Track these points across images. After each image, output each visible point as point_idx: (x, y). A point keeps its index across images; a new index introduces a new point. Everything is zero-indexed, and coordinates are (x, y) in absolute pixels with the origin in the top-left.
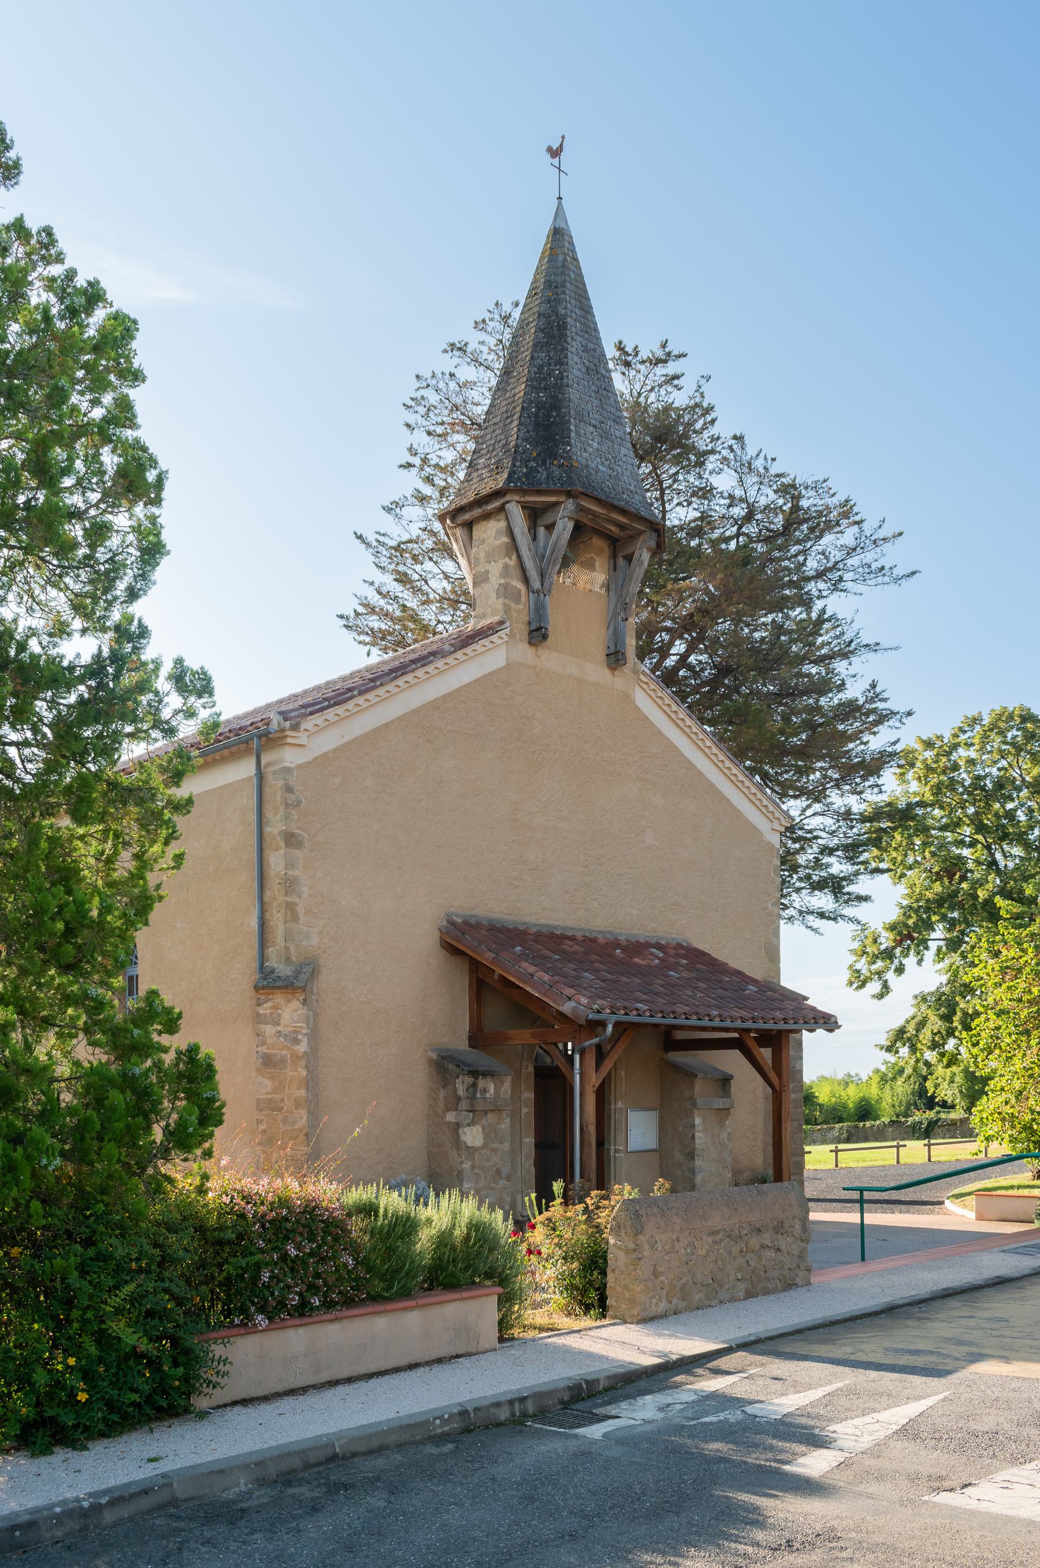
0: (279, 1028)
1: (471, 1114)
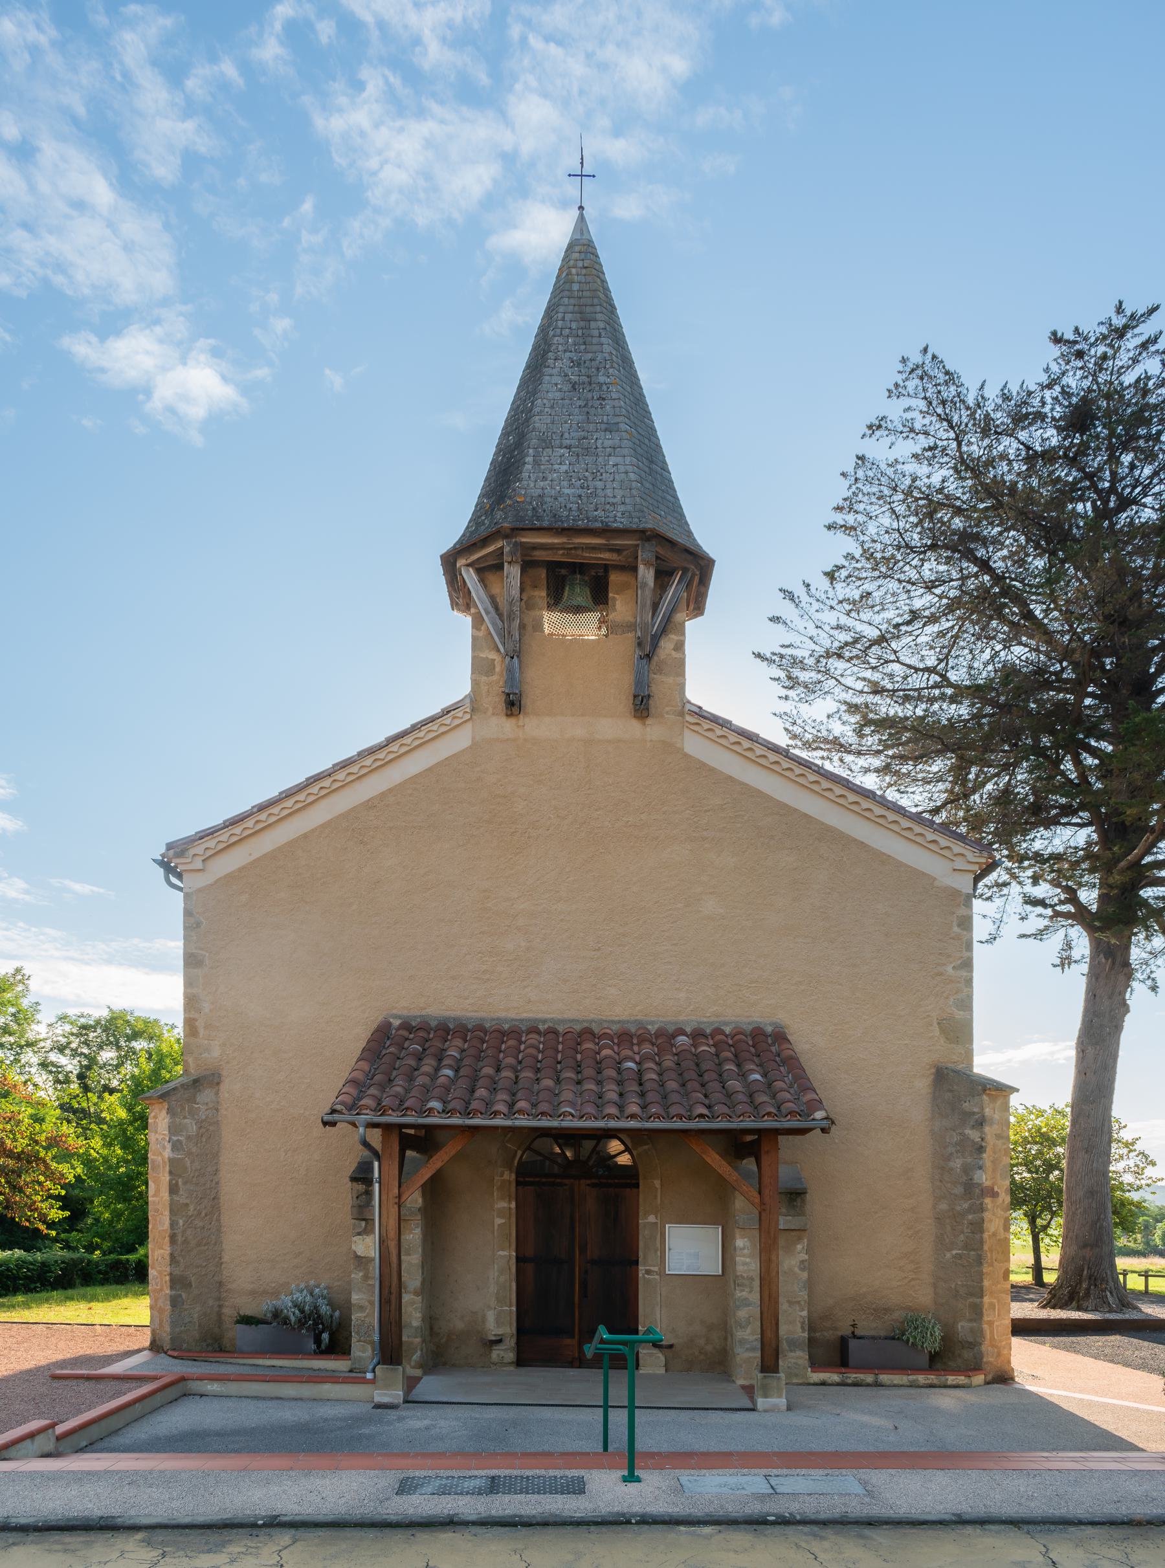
1: (363, 1224)
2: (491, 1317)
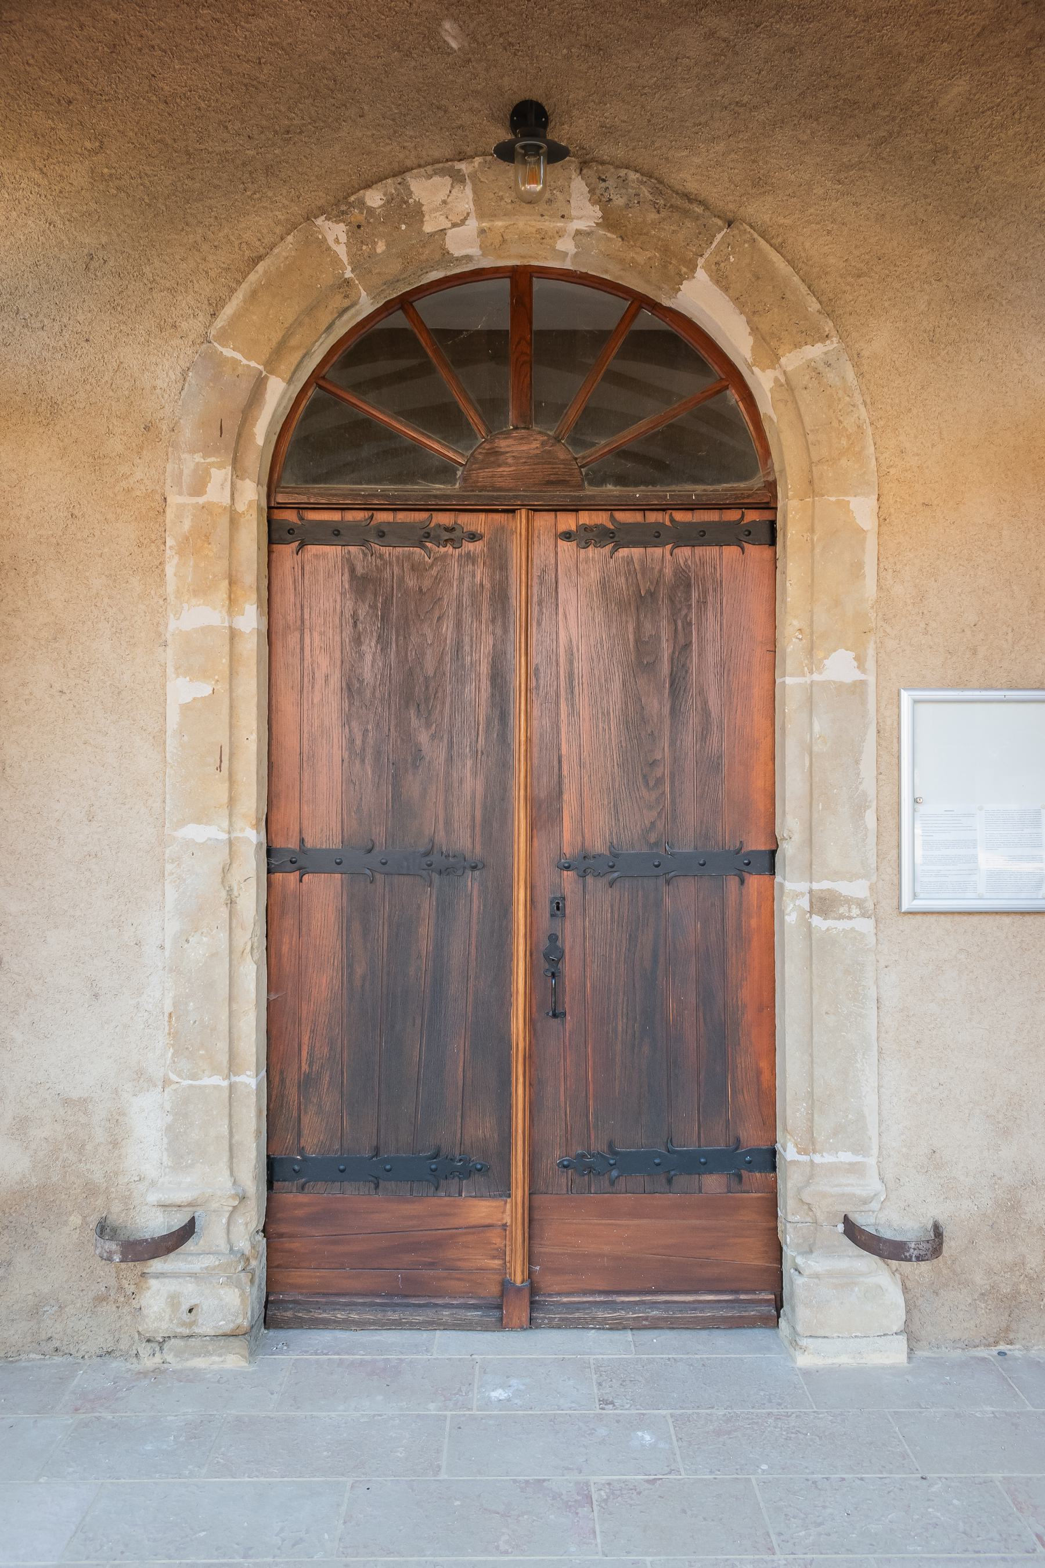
2: (147, 1118)
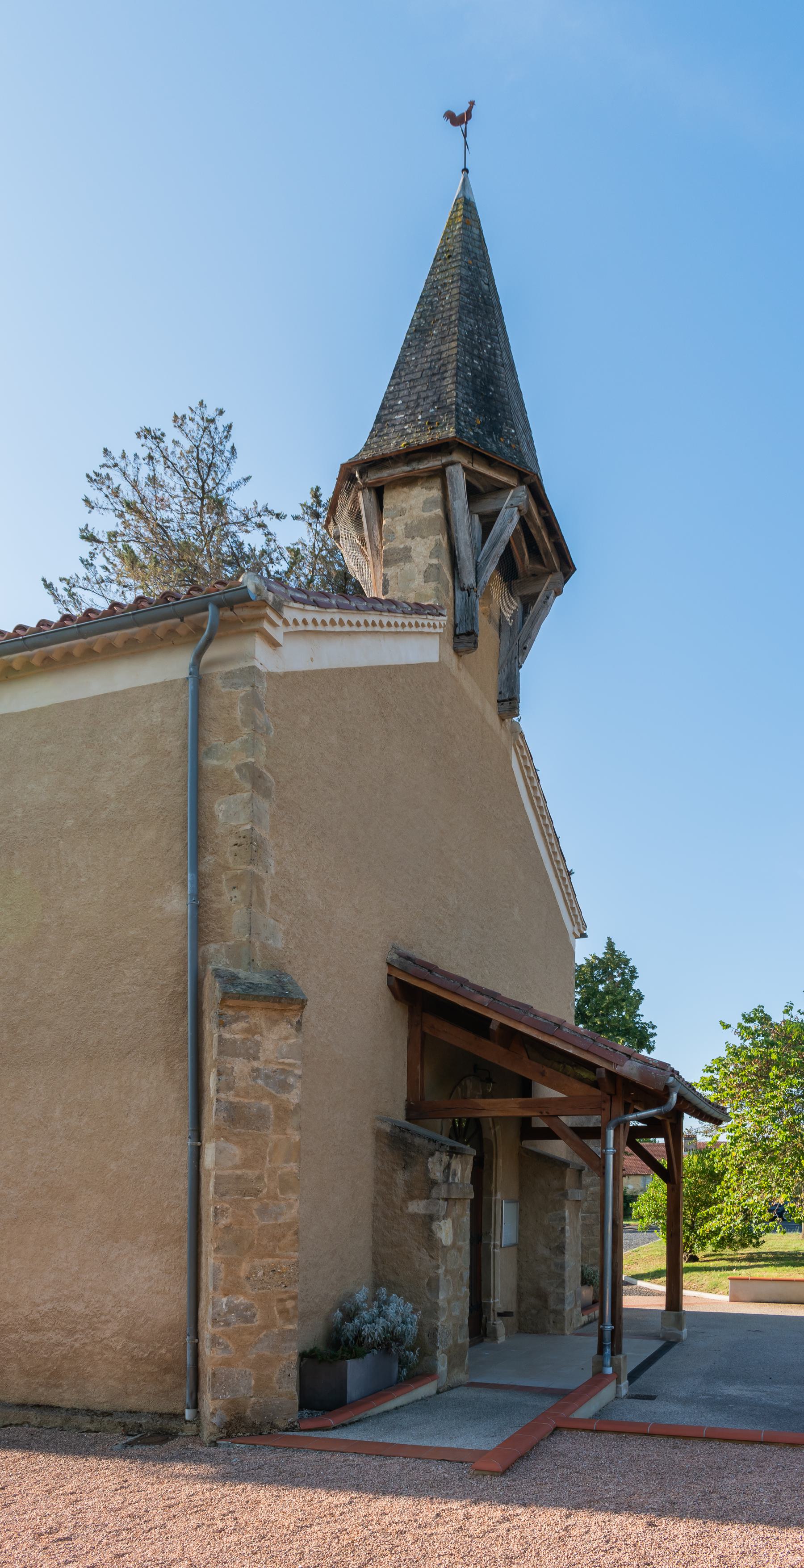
0: (256, 1064)
